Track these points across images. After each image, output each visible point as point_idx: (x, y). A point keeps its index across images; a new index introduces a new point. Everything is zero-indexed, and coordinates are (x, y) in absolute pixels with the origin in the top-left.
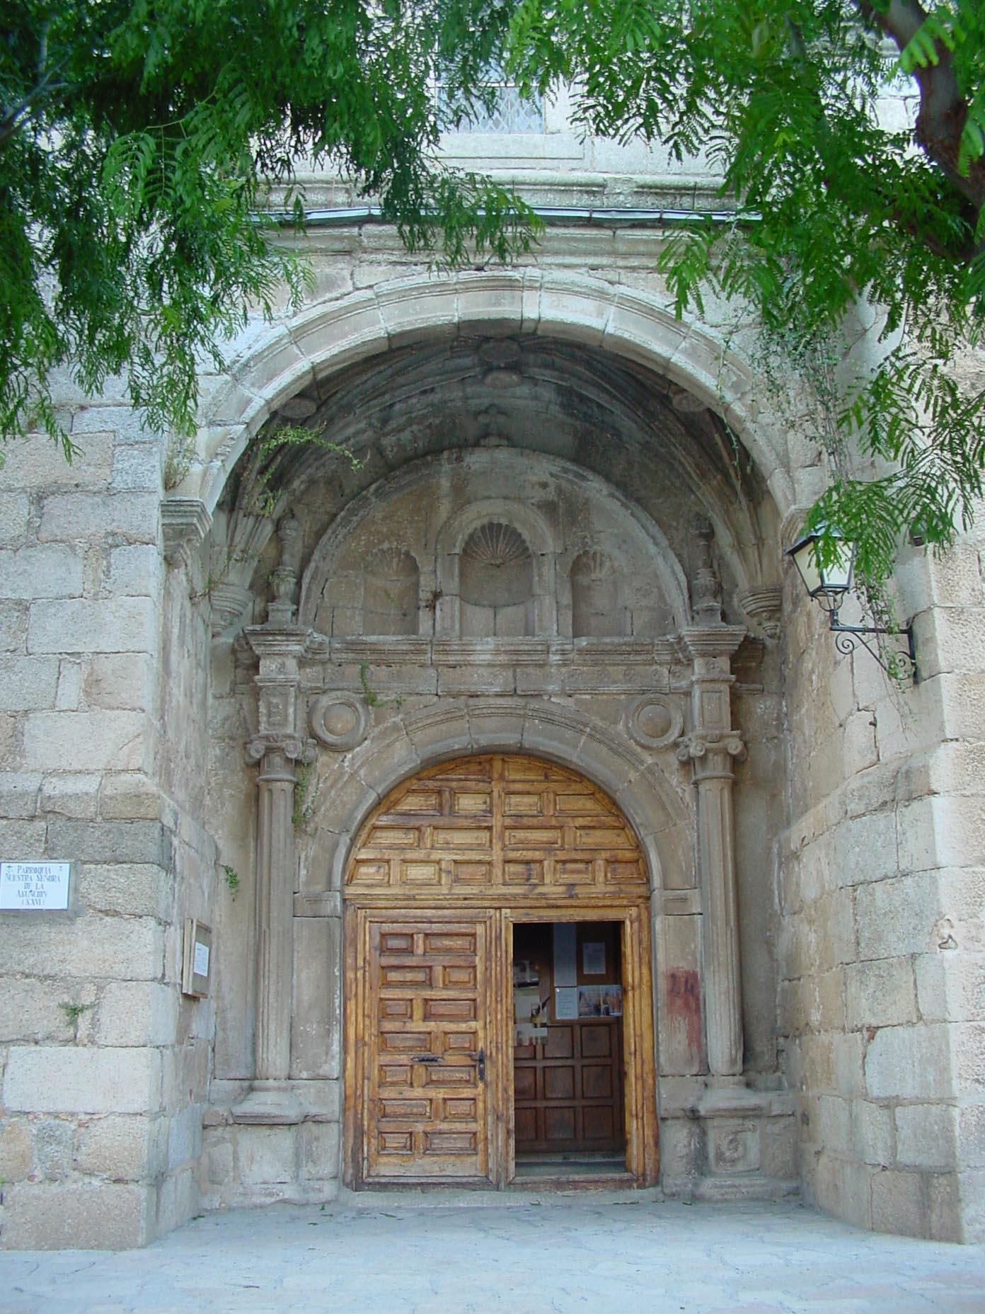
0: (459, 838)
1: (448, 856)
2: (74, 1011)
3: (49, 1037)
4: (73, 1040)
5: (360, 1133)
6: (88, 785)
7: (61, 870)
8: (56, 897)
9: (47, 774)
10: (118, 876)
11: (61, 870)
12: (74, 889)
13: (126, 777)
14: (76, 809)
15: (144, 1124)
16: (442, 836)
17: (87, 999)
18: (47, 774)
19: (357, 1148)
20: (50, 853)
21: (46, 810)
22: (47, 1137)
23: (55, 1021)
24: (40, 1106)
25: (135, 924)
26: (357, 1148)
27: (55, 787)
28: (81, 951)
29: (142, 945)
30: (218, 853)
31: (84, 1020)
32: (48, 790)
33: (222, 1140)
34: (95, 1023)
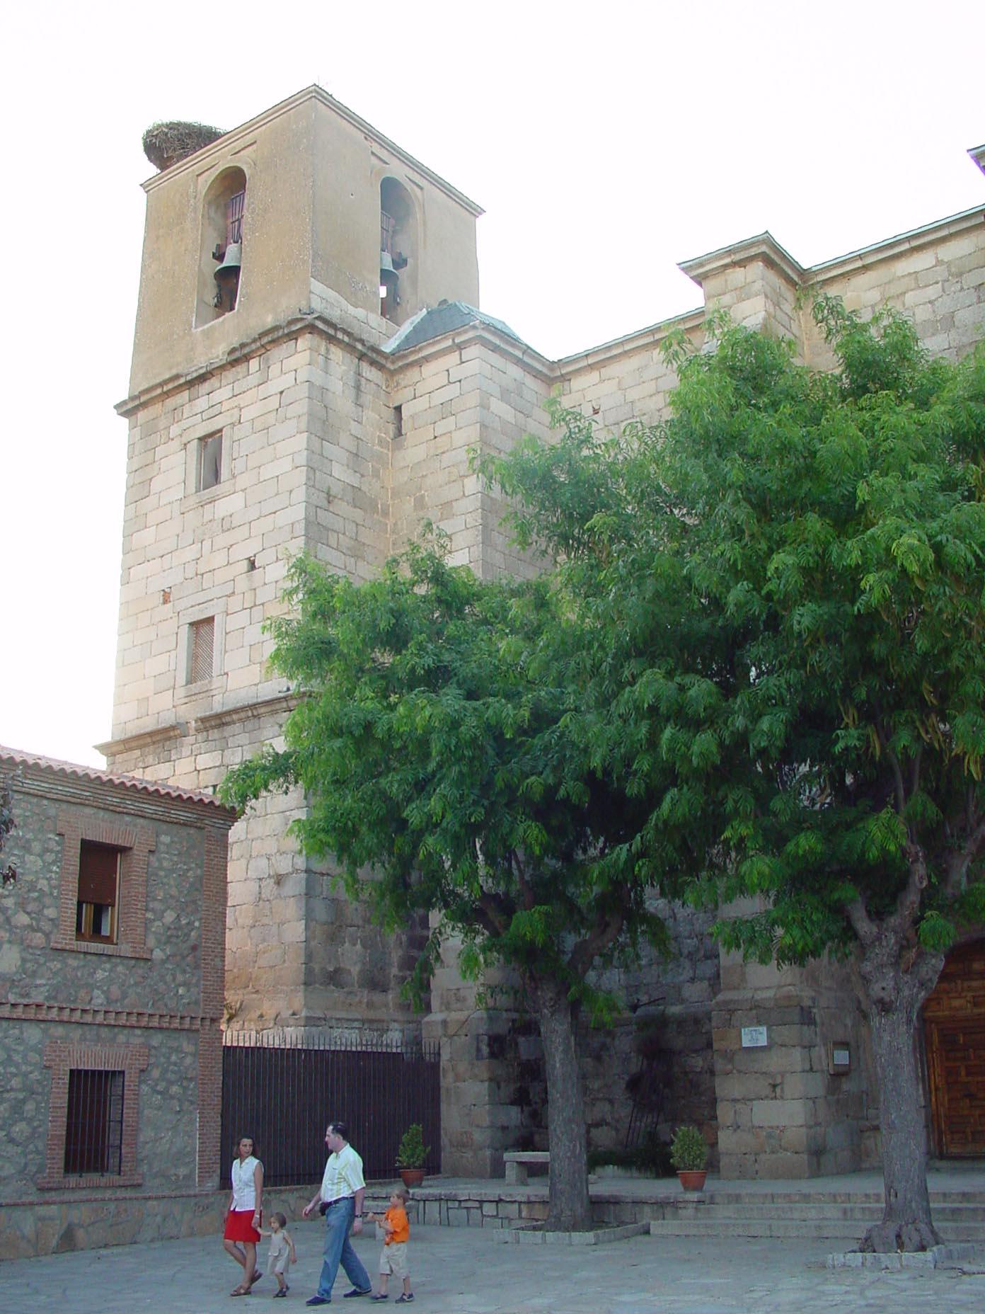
0: (975, 984)
1: (970, 994)
2: (774, 1086)
3: (767, 1097)
4: (775, 1098)
5: (940, 1133)
6: (770, 994)
7: (763, 1029)
8: (763, 1041)
9: (756, 989)
10: (784, 1030)
11: (763, 1029)
12: (769, 1037)
13: (786, 989)
14: (767, 1005)
15: (804, 1130)
16: (966, 984)
17: (778, 1081)
18: (756, 989)
19: (940, 1140)
20: (759, 1023)
21: (756, 1006)
22: (770, 1136)
23: (768, 1091)
24: (766, 1124)
25: (793, 1050)
26: (940, 1140)
27: (760, 995)
28: (774, 1062)
29: (797, 1057)
30: (859, 1002)
31: (778, 1090)
32: (756, 997)
33: (869, 1137)
34: (782, 1090)
